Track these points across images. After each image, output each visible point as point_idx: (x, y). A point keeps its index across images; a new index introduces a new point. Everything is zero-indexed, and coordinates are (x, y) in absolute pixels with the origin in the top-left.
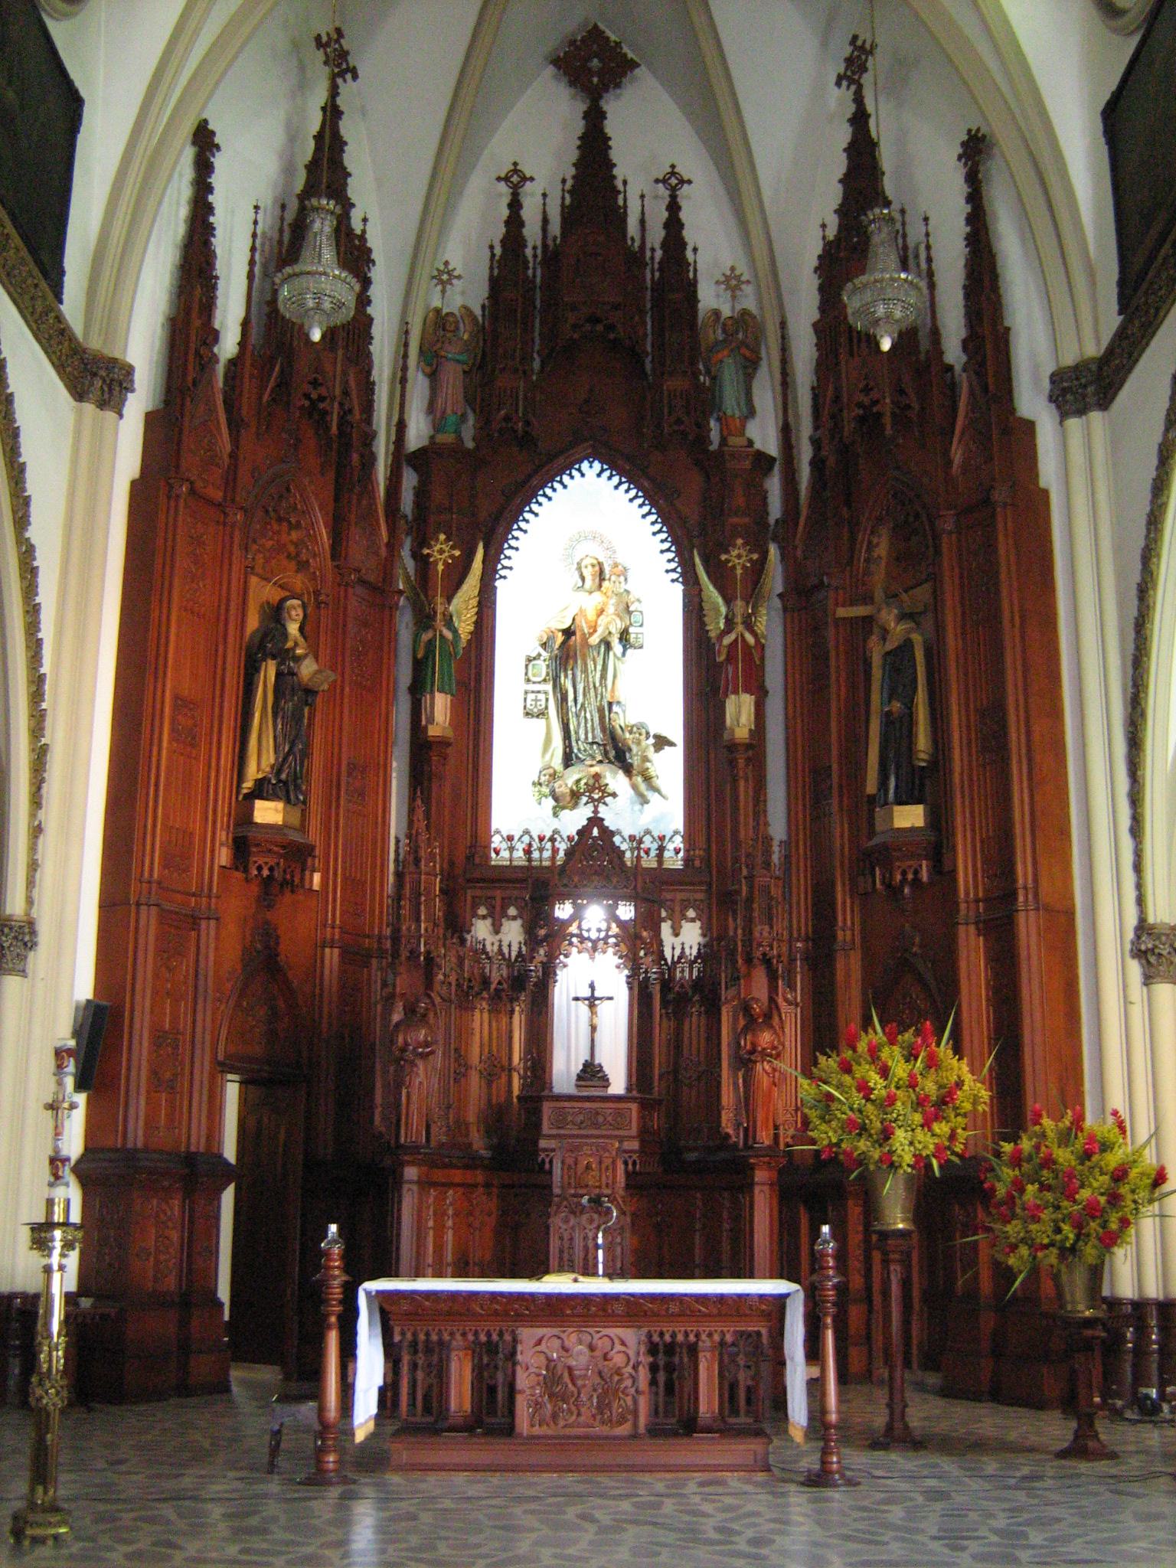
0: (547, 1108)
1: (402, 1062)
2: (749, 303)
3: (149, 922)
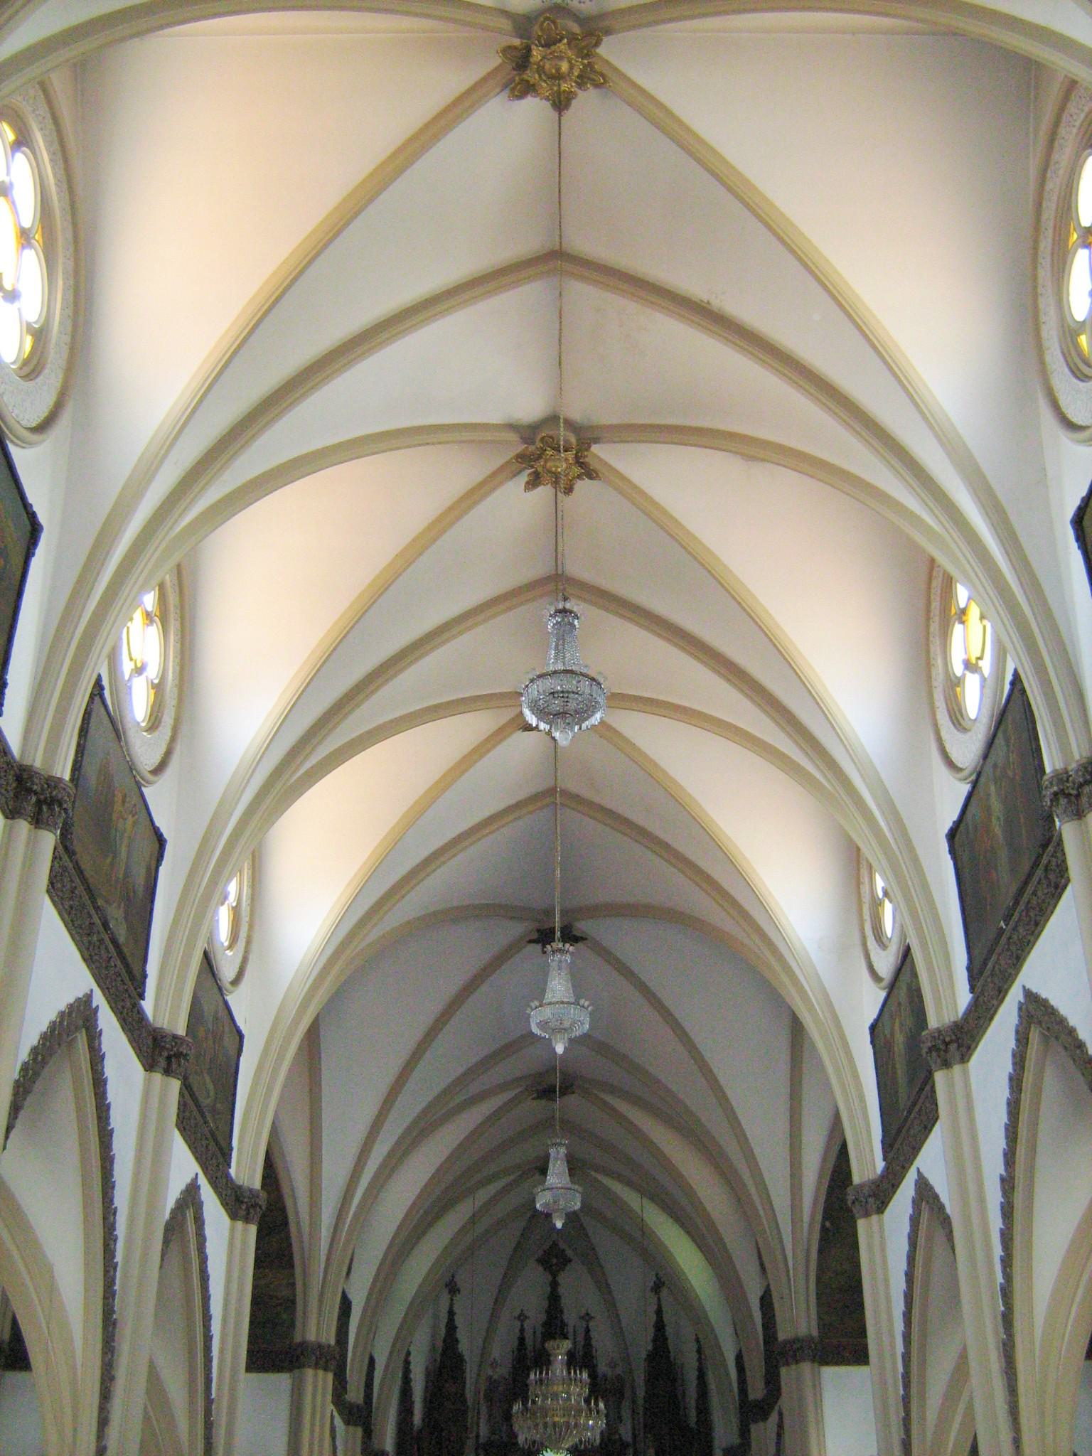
2: (619, 1371)
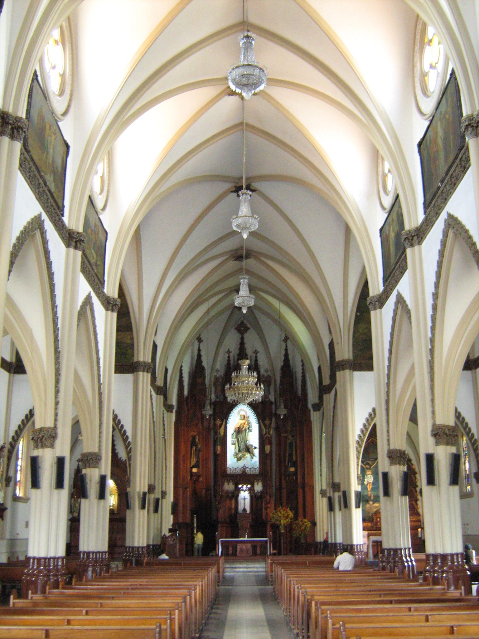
0: (238, 516)
1: (217, 510)
2: (269, 373)
3: (181, 490)
